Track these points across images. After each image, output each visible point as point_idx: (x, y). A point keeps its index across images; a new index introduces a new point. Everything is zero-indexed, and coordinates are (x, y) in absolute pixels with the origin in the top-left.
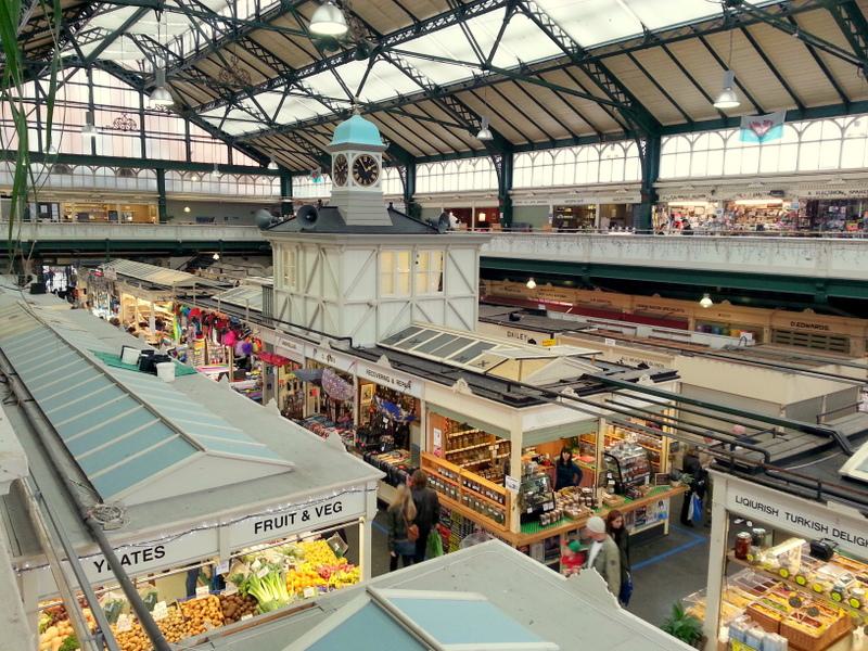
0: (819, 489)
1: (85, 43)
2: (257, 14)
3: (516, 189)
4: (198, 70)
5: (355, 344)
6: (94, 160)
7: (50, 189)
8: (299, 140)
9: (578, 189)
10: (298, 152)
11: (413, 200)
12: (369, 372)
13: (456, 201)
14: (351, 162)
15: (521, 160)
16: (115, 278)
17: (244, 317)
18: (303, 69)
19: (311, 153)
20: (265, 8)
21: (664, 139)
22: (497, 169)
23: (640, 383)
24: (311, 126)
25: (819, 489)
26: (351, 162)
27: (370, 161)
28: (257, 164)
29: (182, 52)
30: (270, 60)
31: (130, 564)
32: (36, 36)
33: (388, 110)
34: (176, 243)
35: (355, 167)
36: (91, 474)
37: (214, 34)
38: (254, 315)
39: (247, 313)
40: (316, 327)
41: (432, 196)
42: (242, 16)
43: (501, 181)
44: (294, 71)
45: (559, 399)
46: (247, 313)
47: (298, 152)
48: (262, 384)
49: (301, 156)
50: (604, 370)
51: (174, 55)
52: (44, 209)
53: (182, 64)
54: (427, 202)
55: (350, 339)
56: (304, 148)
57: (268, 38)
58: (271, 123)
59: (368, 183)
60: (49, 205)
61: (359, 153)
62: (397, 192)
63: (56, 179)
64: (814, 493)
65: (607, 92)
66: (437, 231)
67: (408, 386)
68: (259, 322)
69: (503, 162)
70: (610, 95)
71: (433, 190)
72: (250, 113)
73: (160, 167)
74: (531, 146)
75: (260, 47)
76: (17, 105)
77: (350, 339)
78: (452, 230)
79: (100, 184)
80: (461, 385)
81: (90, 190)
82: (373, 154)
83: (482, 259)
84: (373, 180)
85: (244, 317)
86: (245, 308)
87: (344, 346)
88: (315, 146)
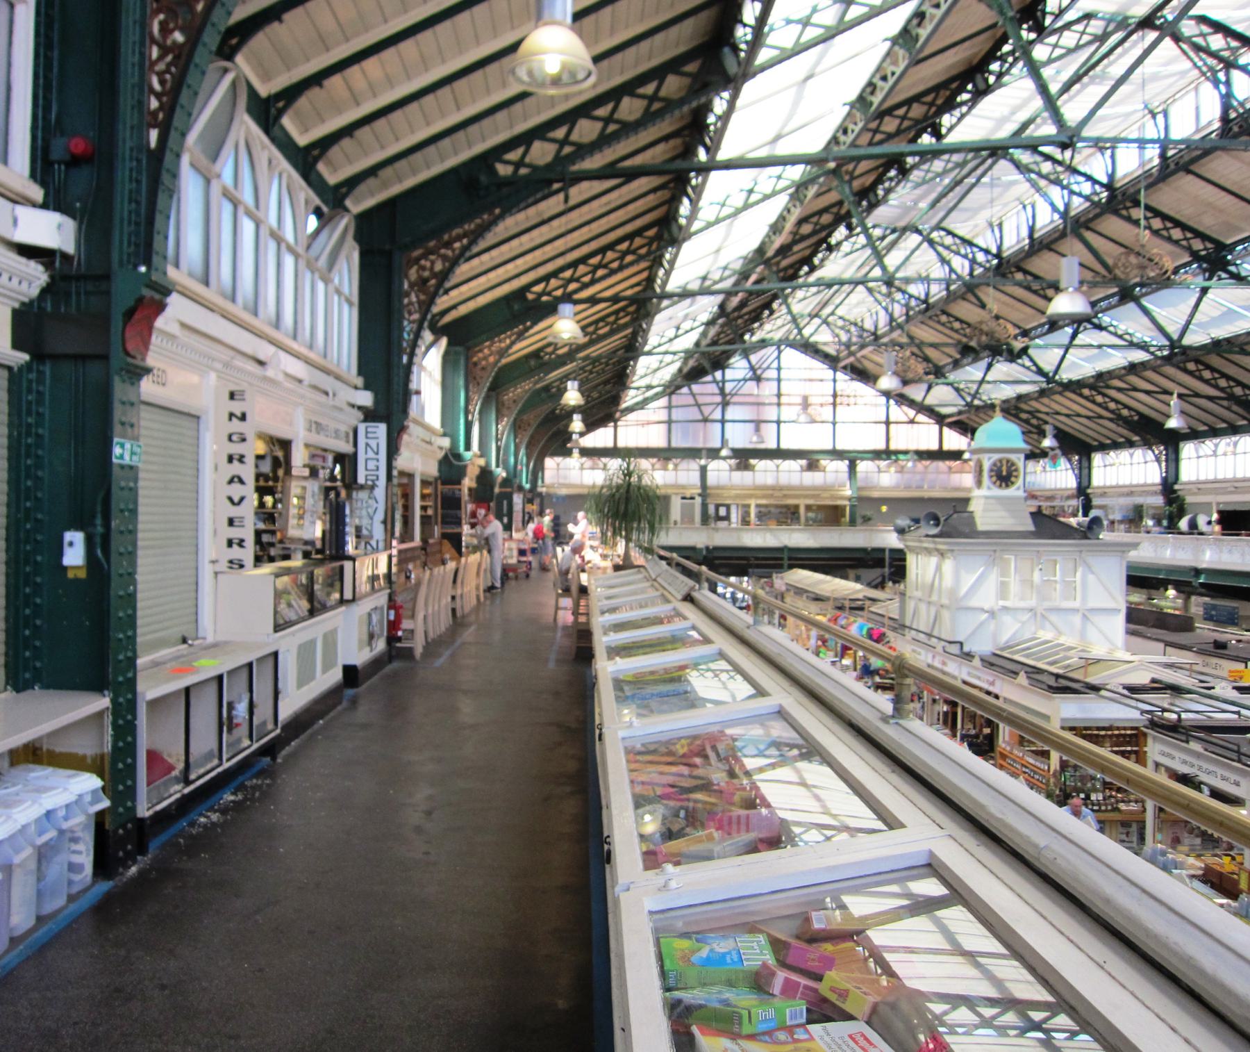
0: (1238, 752)
1: (1050, 61)
2: (1225, 119)
3: (1186, 483)
4: (949, 315)
5: (966, 649)
6: (778, 454)
7: (733, 487)
8: (1207, 374)
9: (1237, 484)
10: (1197, 395)
11: (1175, 491)
12: (969, 674)
13: (1231, 493)
14: (986, 465)
15: (1097, 459)
16: (784, 588)
17: (883, 625)
18: (1035, 328)
19: (1232, 397)
20: (1041, 229)
21: (1181, 445)
23: (1217, 691)
24: (1120, 378)
25: (1238, 752)
26: (986, 465)
27: (1011, 464)
29: (999, 248)
30: (1176, 234)
31: (850, 1036)
32: (796, 248)
33: (1092, 387)
34: (864, 550)
35: (991, 470)
36: (248, 60)
37: (972, 270)
38: (891, 623)
39: (886, 621)
40: (935, 633)
41: (1201, 486)
42: (1176, 135)
43: (1079, 478)
44: (1221, 247)
45: (1103, 693)
46: (886, 621)
47: (1197, 395)
48: (227, 365)
50: (1201, 681)
51: (987, 252)
52: (722, 512)
53: (927, 309)
54: (1195, 494)
55: (961, 644)
56: (1107, 409)
57: (1168, 198)
58: (1050, 380)
59: (1007, 486)
60: (728, 507)
61: (996, 457)
62: (1069, 486)
63: (743, 478)
64: (1234, 756)
65: (1216, 387)
66: (1086, 537)
67: (992, 684)
68: (894, 629)
69: (1080, 461)
70: (1222, 390)
71: (1202, 478)
72: (1115, 334)
73: (852, 459)
74: (1103, 448)
75: (957, 319)
76: (881, 245)
77: (961, 644)
78: (1201, 534)
79: (784, 480)
80: (1022, 679)
81: (773, 488)
82: (1013, 457)
83: (1130, 567)
85: (883, 625)
86: (883, 616)
87: (955, 649)
88: (1126, 407)
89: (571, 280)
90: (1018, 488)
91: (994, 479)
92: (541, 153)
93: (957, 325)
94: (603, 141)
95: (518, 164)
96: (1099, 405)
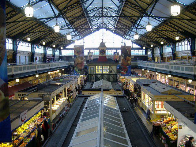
22: (189, 44)
49: (155, 38)
56: (175, 29)
75: (91, 10)
92: (27, 31)
93: (92, 11)
94: (32, 30)
95: (25, 32)
96: (173, 28)
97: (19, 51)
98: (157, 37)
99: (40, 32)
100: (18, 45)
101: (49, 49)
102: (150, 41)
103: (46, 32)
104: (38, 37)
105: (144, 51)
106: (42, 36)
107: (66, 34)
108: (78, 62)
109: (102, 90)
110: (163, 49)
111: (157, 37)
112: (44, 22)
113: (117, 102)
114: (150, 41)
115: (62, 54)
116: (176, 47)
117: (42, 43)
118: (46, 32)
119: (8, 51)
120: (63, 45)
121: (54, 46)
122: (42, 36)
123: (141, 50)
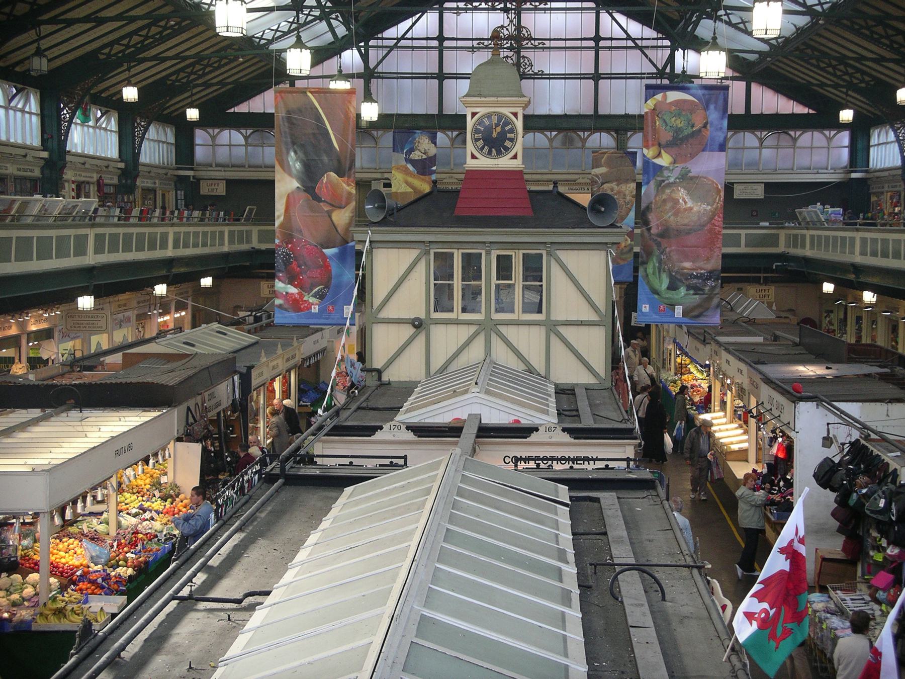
28: (800, 109)
35: (476, 131)
59: (499, 153)
84: (507, 149)
89: (192, 73)
90: (515, 157)
91: (480, 143)
97: (144, 165)
98: (880, 60)
99: (94, 20)
100: (143, 138)
101: (153, 132)
102: (887, 55)
103: (188, 62)
104: (88, 48)
105: (844, 138)
106: (117, 41)
107: (269, 35)
108: (672, 220)
109: (470, 433)
110: (868, 147)
111: (880, 60)
112: (261, 38)
113: (587, 631)
114: (887, 55)
115: (200, 153)
116: (872, 150)
117: (120, 92)
118: (188, 62)
119: (146, 169)
120: (207, 85)
121: (130, 94)
122: (111, 44)
123: (815, 138)
